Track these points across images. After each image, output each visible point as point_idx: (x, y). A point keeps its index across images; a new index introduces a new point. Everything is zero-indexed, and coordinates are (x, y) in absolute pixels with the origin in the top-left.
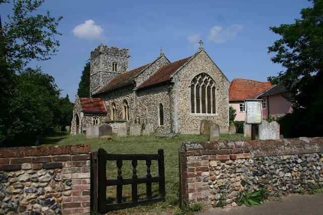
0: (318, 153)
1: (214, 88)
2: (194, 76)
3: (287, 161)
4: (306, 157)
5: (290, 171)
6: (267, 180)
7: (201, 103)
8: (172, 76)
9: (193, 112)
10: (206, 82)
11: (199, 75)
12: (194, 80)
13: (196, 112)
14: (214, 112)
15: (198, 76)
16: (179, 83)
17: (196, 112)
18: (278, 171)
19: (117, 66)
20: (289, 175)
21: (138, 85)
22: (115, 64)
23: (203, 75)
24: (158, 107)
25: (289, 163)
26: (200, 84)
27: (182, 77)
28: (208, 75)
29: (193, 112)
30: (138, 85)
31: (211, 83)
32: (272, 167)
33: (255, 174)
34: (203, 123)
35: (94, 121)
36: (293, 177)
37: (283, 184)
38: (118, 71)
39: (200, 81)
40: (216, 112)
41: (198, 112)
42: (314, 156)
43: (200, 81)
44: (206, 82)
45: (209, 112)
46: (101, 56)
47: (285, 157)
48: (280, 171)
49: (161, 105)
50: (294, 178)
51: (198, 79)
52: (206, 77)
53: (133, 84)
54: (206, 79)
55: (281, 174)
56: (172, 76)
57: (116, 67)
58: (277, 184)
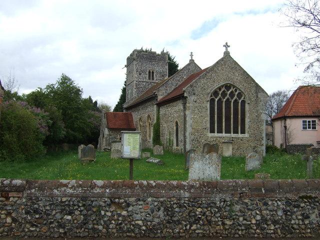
0: (108, 198)
1: (243, 102)
2: (216, 86)
3: (67, 203)
4: (92, 202)
5: (70, 214)
6: (40, 221)
7: (224, 120)
8: (184, 89)
9: (212, 131)
10: (232, 95)
11: (222, 86)
12: (215, 93)
13: (216, 132)
14: (243, 132)
15: (220, 89)
16: (193, 98)
17: (216, 132)
18: (54, 212)
19: (154, 75)
20: (69, 217)
21: (160, 98)
23: (228, 87)
24: (174, 125)
25: (69, 205)
26: (228, 99)
27: (198, 90)
28: (234, 87)
30: (160, 98)
31: (240, 95)
32: (48, 208)
33: (27, 213)
34: (206, 148)
36: (74, 220)
37: (61, 226)
38: (155, 79)
39: (224, 94)
40: (246, 132)
41: (220, 131)
42: (103, 201)
43: (224, 94)
44: (232, 95)
45: (236, 132)
46: (135, 61)
47: (64, 199)
48: (57, 213)
50: (75, 221)
51: (220, 92)
53: (154, 97)
54: (232, 92)
55: (58, 216)
56: (184, 89)
58: (54, 225)
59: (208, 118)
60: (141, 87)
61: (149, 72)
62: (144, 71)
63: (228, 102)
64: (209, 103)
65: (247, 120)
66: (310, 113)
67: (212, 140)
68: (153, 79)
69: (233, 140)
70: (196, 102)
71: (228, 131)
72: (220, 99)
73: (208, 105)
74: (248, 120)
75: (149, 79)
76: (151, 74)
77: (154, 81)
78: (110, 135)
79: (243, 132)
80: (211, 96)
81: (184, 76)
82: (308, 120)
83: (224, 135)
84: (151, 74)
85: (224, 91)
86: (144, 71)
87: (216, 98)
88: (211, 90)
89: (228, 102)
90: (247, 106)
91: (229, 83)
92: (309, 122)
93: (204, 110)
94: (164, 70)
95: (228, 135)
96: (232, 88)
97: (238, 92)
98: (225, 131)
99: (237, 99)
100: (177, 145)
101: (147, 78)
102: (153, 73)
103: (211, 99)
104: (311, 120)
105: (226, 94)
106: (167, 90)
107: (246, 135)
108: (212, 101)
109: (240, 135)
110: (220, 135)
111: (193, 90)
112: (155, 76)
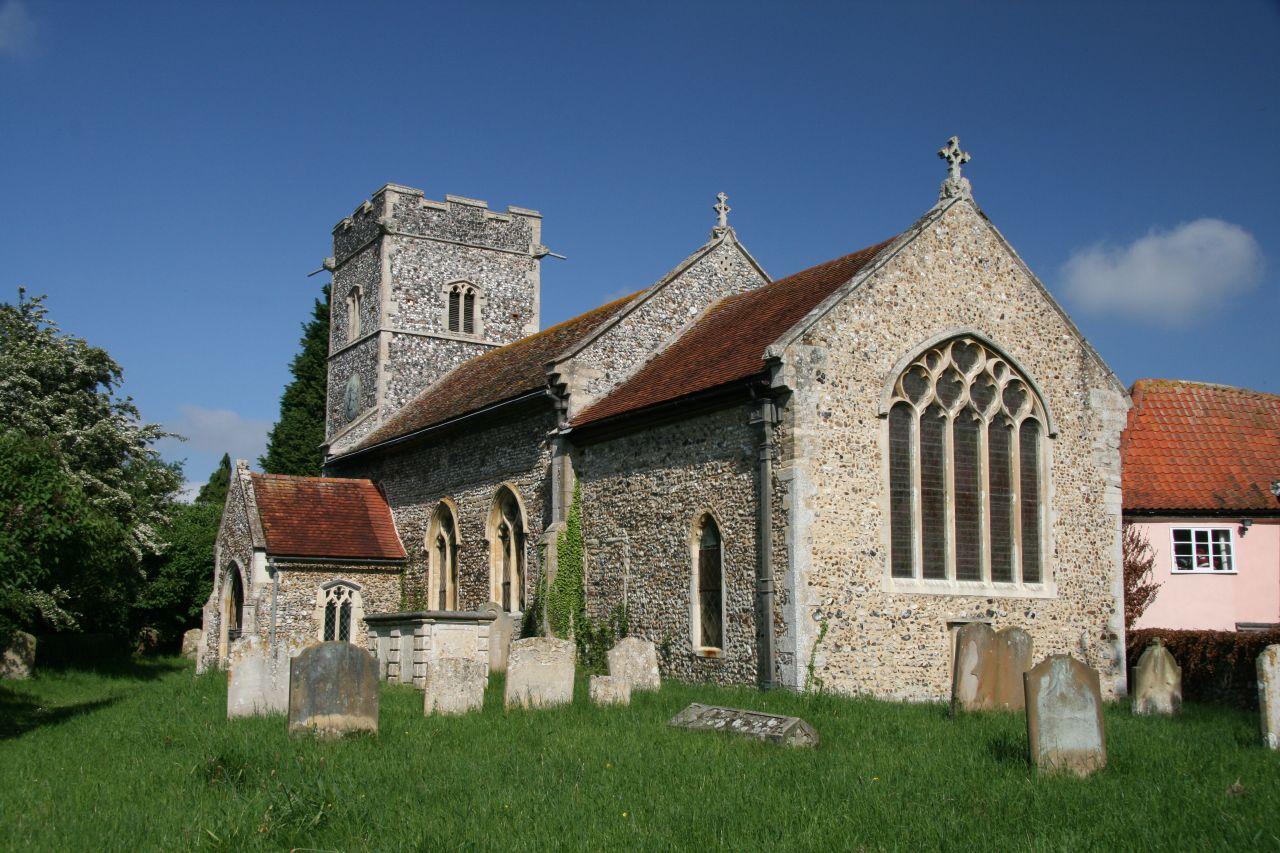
1: (1030, 425)
2: (914, 345)
10: (983, 389)
11: (942, 345)
12: (914, 377)
14: (1032, 575)
15: (931, 355)
22: (464, 291)
23: (965, 347)
27: (835, 360)
28: (992, 351)
29: (902, 568)
31: (1014, 396)
35: (331, 607)
39: (949, 386)
43: (949, 386)
44: (983, 389)
49: (709, 524)
52: (983, 363)
53: (545, 401)
54: (983, 377)
57: (469, 313)
59: (884, 502)
60: (415, 365)
61: (454, 295)
62: (427, 291)
63: (966, 423)
64: (885, 423)
65: (1048, 516)
66: (1204, 501)
67: (903, 610)
68: (469, 328)
69: (990, 613)
70: (827, 416)
71: (968, 570)
72: (933, 409)
73: (882, 433)
74: (1054, 517)
75: (454, 326)
76: (461, 305)
77: (477, 336)
78: (280, 590)
79: (1032, 575)
80: (895, 394)
81: (687, 303)
82: (1194, 527)
83: (951, 584)
84: (461, 305)
85: (949, 372)
86: (427, 291)
87: (915, 400)
88: (894, 361)
89: (966, 423)
90: (1045, 447)
91: (970, 336)
92: (1201, 536)
93: (863, 459)
94: (522, 289)
95: (969, 587)
96: (982, 356)
97: (1007, 375)
98: (959, 570)
99: (1007, 410)
100: (713, 636)
101: (445, 321)
102: (470, 298)
103: (897, 405)
104: (1208, 527)
105: (924, 382)
106: (611, 365)
107: (1046, 588)
108: (900, 413)
109: (1019, 589)
110: (935, 586)
111: (816, 358)
112: (477, 314)
